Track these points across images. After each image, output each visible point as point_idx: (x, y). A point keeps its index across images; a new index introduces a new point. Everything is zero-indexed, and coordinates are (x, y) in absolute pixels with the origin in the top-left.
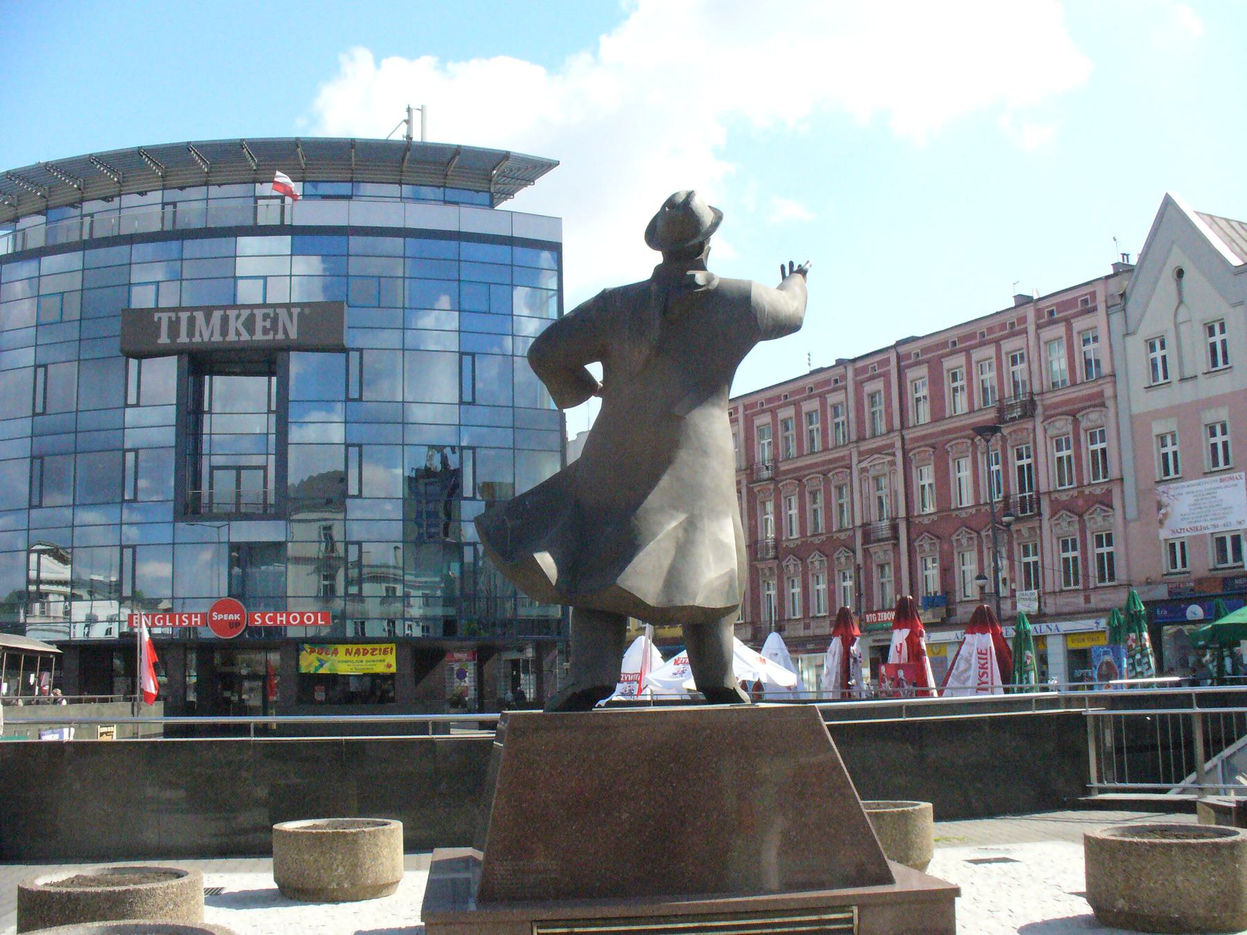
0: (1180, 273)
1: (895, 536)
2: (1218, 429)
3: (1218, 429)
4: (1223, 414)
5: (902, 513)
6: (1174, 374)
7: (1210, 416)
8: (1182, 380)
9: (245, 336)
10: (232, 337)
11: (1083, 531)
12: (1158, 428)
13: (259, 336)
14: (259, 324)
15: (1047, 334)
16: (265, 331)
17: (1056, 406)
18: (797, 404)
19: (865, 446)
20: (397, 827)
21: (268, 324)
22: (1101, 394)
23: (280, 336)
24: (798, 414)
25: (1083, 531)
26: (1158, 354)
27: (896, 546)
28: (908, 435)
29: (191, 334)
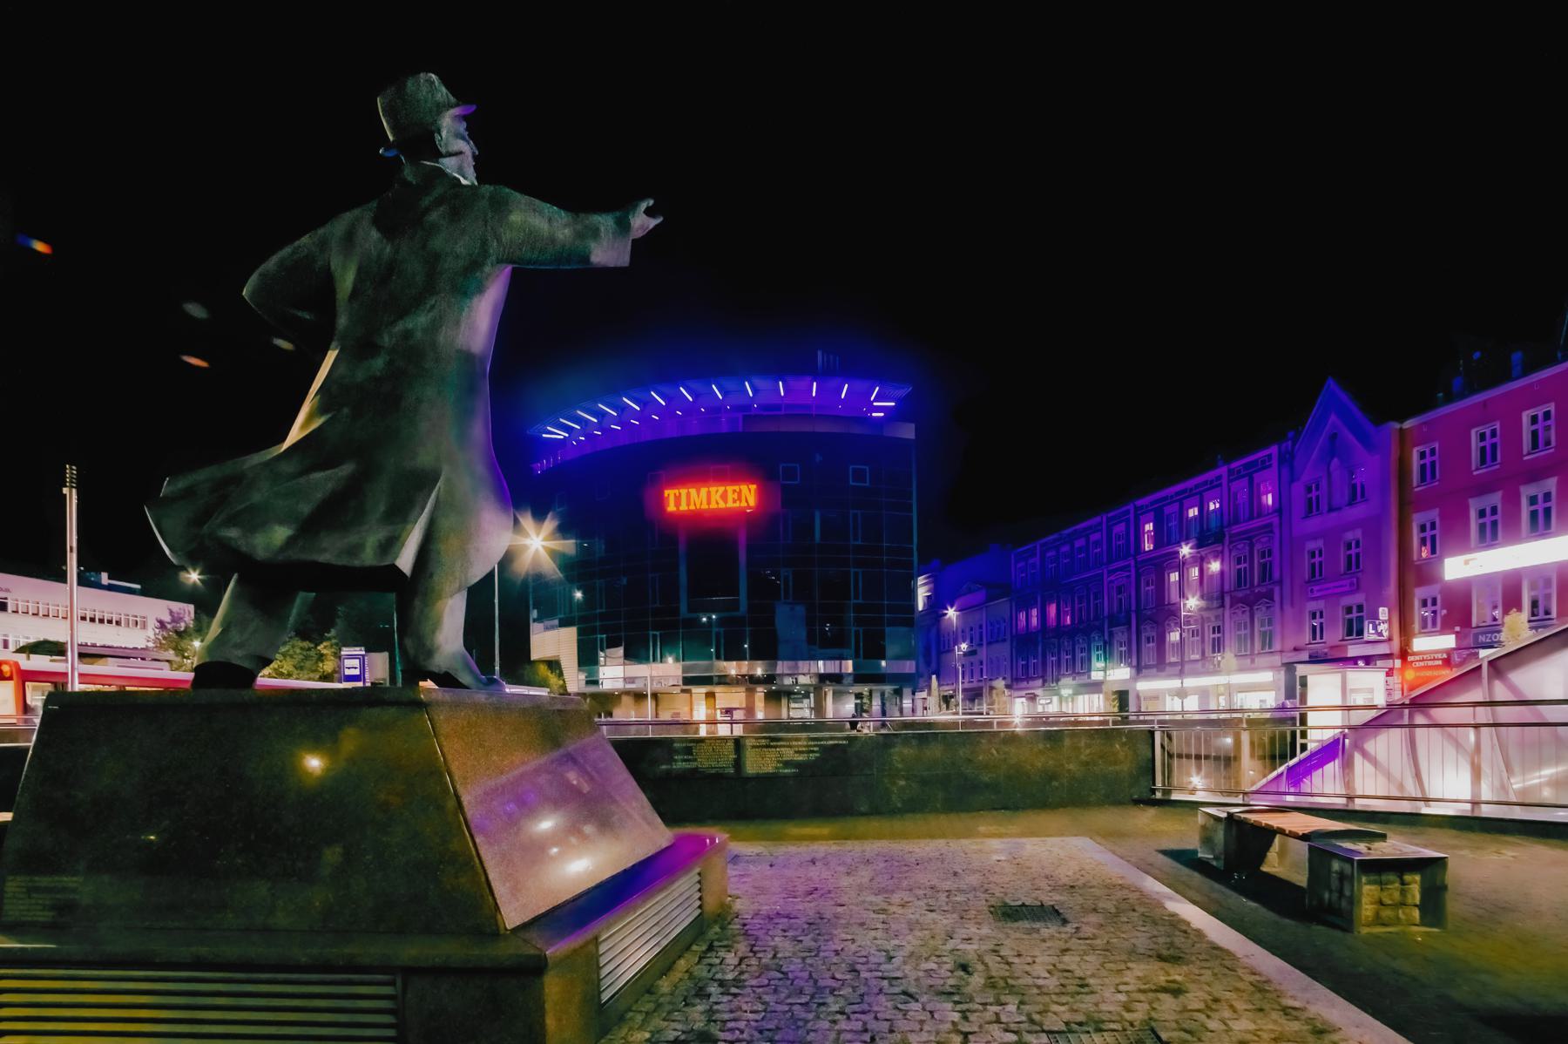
8: (1331, 510)
9: (722, 505)
10: (713, 506)
12: (1311, 545)
13: (730, 505)
14: (731, 496)
23: (744, 504)
27: (1129, 629)
28: (1139, 558)
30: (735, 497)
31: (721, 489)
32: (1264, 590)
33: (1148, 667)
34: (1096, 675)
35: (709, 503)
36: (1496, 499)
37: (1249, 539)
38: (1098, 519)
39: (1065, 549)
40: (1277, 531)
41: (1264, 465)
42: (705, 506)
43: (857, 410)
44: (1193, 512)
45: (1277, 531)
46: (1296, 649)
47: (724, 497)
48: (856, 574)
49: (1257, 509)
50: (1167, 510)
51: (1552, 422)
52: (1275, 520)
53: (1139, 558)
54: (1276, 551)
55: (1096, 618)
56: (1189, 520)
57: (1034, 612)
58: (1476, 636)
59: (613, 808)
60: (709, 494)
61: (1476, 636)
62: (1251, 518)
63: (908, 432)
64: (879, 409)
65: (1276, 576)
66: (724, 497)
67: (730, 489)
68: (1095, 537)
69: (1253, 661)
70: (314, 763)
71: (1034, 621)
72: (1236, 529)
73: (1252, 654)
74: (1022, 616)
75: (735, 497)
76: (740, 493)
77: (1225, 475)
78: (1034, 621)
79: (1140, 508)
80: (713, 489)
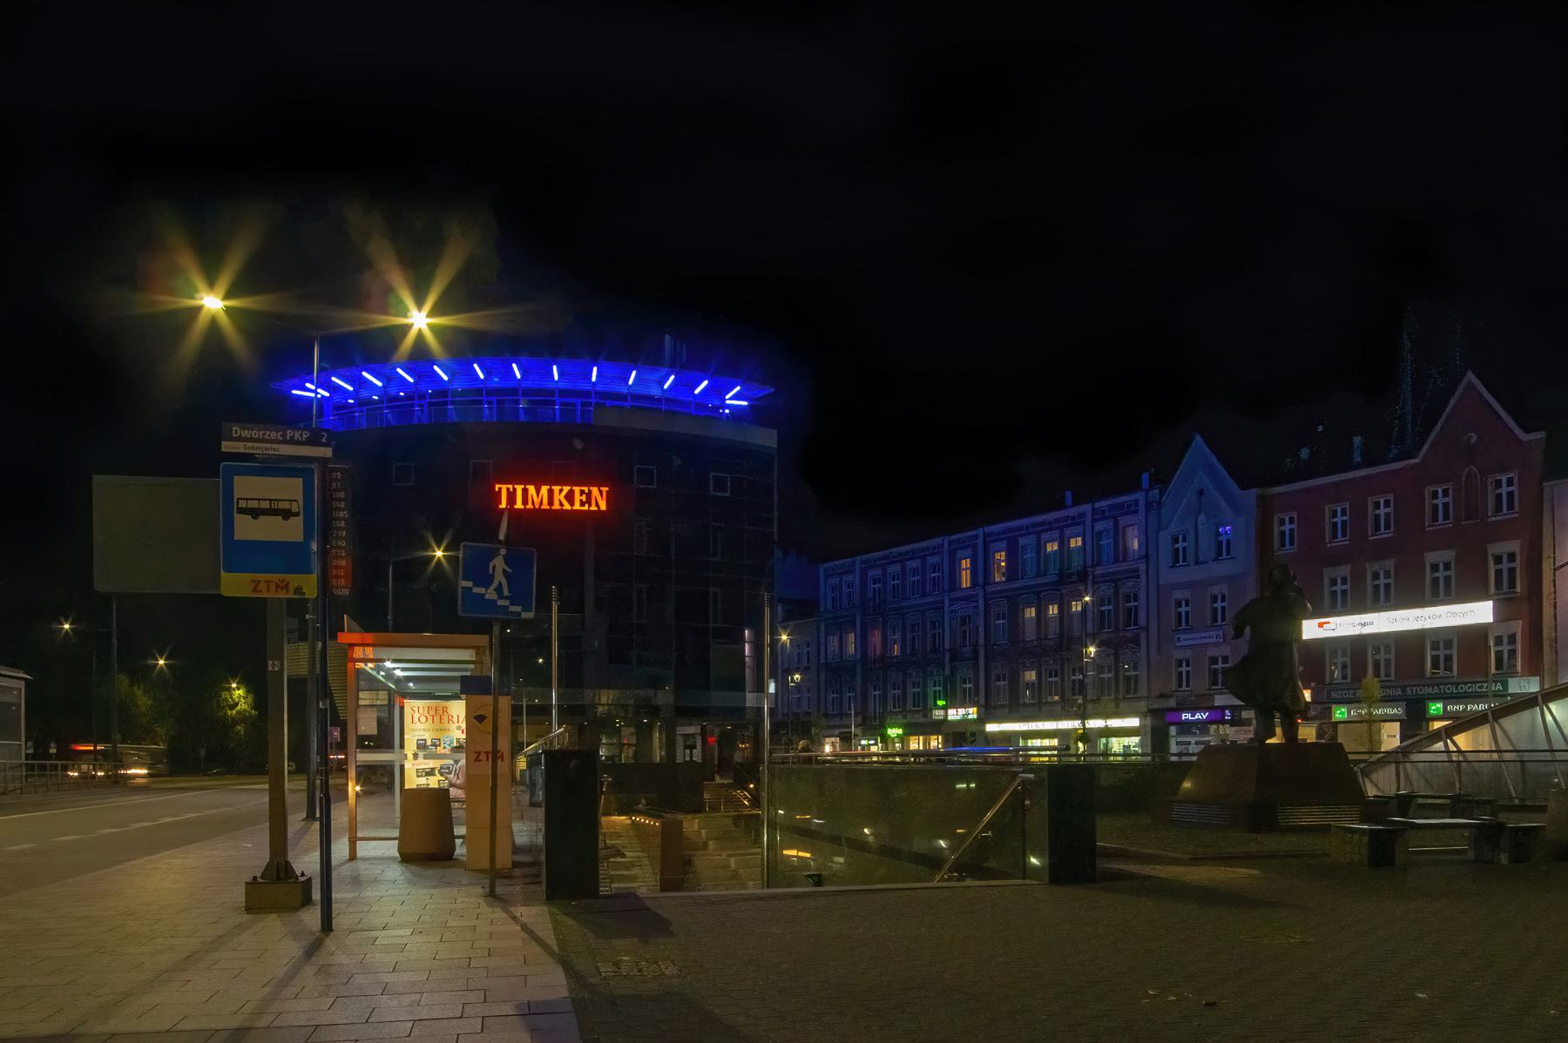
0: (1201, 492)
1: (976, 659)
2: (1505, 640)
3: (1505, 640)
4: (1224, 588)
5: (981, 642)
6: (1191, 558)
7: (1215, 590)
8: (1197, 563)
9: (567, 506)
10: (556, 506)
11: (1116, 593)
12: (1178, 595)
13: (577, 507)
15: (1099, 526)
16: (582, 504)
17: (1103, 576)
18: (903, 562)
19: (954, 595)
20: (603, 819)
21: (584, 498)
22: (1137, 570)
23: (594, 508)
24: (903, 569)
25: (1116, 593)
26: (1180, 545)
27: (976, 667)
28: (990, 589)
29: (525, 502)
30: (965, 580)
31: (566, 489)
32: (1129, 635)
33: (997, 707)
34: (938, 714)
35: (551, 502)
36: (1345, 570)
37: (1115, 581)
38: (938, 540)
39: (896, 568)
40: (1143, 577)
41: (1131, 509)
42: (545, 506)
43: (708, 408)
44: (1052, 547)
45: (1143, 577)
46: (1162, 696)
47: (570, 497)
48: (715, 595)
49: (1121, 554)
50: (1022, 541)
51: (1517, 564)
52: (1142, 567)
53: (990, 589)
54: (1142, 598)
55: (934, 650)
56: (1047, 556)
57: (851, 637)
58: (1329, 692)
59: (369, 893)
60: (551, 492)
61: (1329, 692)
62: (1116, 561)
63: (766, 438)
64: (729, 407)
65: (1142, 622)
66: (570, 497)
67: (577, 489)
68: (932, 560)
69: (1117, 706)
70: (942, 843)
71: (851, 649)
72: (1099, 571)
73: (1116, 699)
74: (834, 643)
75: (965, 580)
76: (589, 495)
77: (1089, 515)
78: (851, 649)
79: (991, 534)
80: (556, 488)
